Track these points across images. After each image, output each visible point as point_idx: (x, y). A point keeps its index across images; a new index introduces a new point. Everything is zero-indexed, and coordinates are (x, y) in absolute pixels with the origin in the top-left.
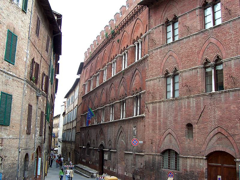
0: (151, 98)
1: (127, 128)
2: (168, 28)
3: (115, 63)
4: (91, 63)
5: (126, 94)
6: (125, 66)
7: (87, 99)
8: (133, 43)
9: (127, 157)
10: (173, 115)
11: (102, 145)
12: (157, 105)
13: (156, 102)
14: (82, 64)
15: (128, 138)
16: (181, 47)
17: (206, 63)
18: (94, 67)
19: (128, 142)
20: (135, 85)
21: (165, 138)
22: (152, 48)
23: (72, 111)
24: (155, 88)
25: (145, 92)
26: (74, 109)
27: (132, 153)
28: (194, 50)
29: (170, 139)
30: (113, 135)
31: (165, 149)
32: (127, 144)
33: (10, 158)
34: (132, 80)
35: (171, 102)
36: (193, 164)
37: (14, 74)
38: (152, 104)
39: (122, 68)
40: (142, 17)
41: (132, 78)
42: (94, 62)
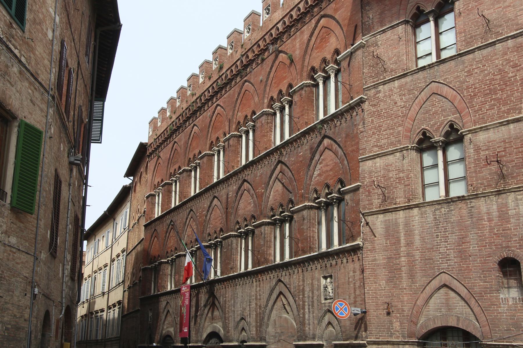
0: (380, 201)
1: (301, 283)
3: (178, 184)
4: (173, 142)
5: (291, 201)
6: (194, 190)
7: (161, 228)
8: (210, 149)
10: (453, 238)
11: (214, 335)
12: (398, 216)
15: (306, 307)
16: (469, 71)
17: (420, 142)
18: (181, 151)
19: (307, 316)
20: (319, 175)
21: (431, 297)
23: (90, 278)
24: (391, 175)
25: (357, 189)
26: (113, 261)
29: (447, 300)
30: (253, 305)
31: (432, 326)
32: (302, 323)
35: (445, 206)
39: (213, 179)
40: (336, 10)
41: (312, 159)
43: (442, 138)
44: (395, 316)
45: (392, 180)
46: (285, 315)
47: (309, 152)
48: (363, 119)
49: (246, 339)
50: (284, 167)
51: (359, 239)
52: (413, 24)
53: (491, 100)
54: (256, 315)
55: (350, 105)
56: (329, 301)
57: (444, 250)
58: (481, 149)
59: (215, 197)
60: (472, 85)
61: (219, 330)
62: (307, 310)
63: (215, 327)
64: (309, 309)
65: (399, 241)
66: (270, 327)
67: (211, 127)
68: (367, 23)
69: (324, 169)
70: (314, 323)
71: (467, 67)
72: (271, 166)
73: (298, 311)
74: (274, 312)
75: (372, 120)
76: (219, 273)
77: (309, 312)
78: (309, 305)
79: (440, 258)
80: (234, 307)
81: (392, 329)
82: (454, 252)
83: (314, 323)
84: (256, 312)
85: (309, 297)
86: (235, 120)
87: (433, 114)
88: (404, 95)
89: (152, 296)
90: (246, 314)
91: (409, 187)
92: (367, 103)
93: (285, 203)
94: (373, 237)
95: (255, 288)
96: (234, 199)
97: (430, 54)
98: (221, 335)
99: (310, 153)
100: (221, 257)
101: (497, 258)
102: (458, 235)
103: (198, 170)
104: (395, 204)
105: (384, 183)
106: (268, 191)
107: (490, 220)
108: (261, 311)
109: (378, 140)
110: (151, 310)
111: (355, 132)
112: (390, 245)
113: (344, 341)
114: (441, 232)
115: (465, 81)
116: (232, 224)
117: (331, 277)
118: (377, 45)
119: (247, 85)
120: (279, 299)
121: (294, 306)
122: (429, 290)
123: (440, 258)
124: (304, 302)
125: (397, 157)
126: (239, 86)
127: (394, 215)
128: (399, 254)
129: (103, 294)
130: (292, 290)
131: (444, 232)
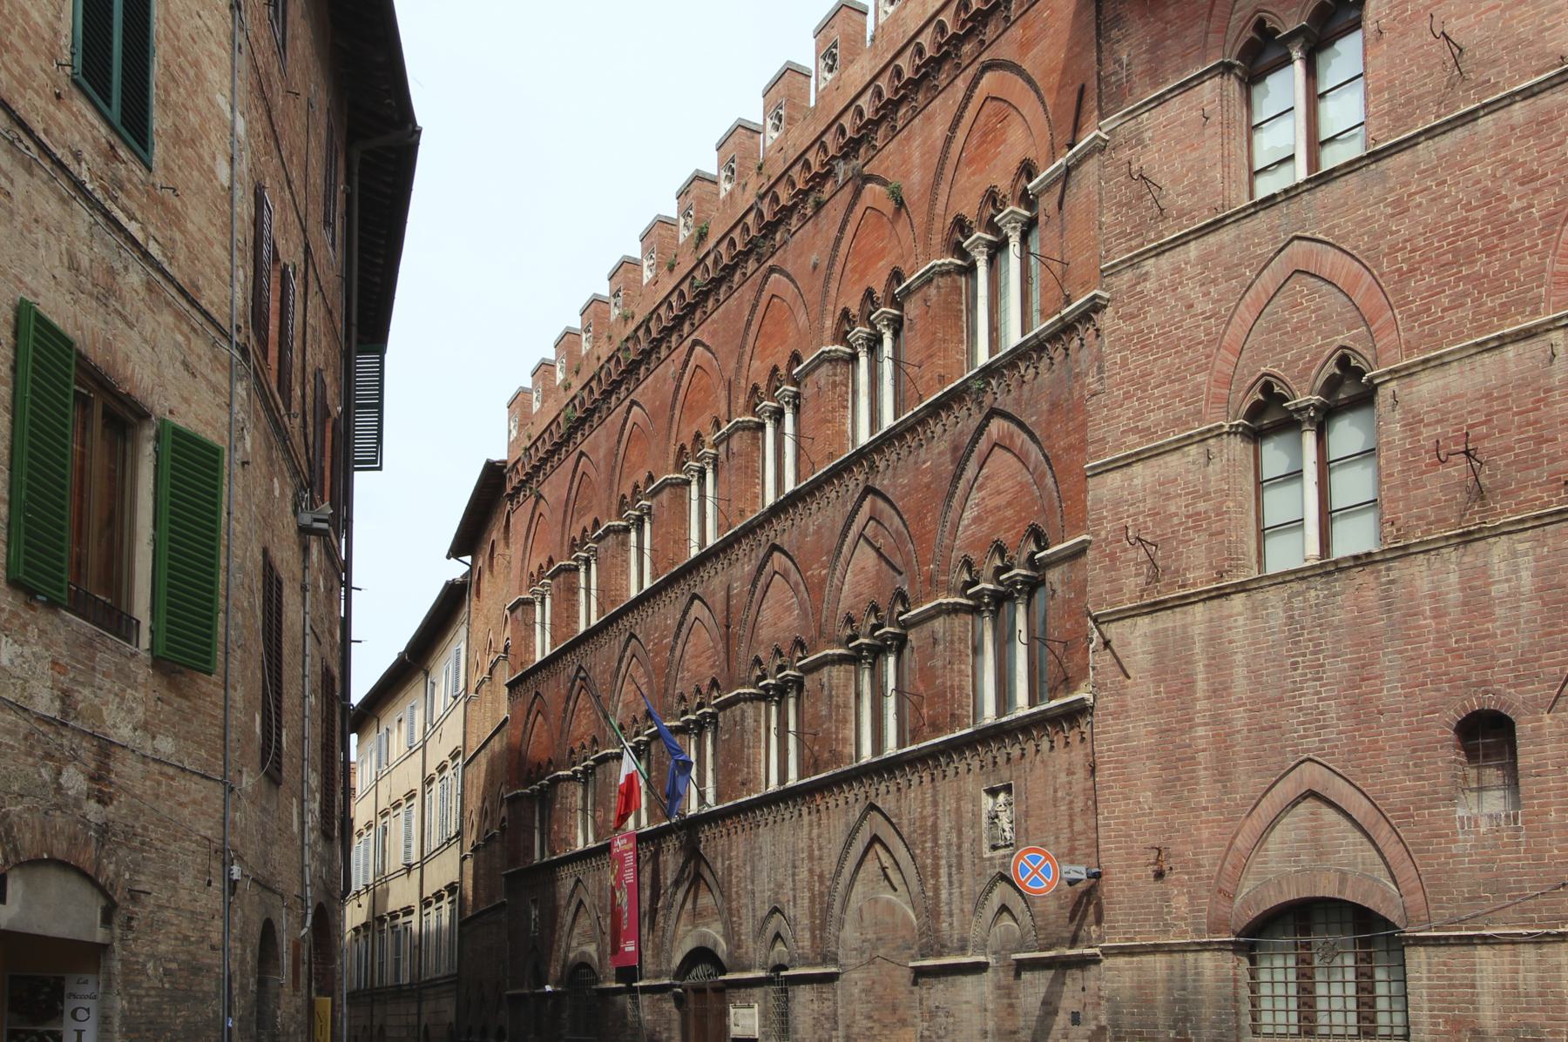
1: (929, 810)
2: (1274, 82)
4: (575, 455)
5: (901, 597)
7: (553, 689)
9: (938, 992)
10: (1337, 669)
11: (702, 955)
13: (1184, 601)
14: (493, 475)
15: (943, 871)
16: (1398, 202)
17: (1256, 411)
18: (598, 476)
19: (944, 895)
20: (977, 520)
21: (1272, 825)
22: (1133, 243)
24: (1173, 509)
25: (1079, 552)
26: (428, 781)
27: (982, 959)
28: (1516, 204)
29: (1316, 831)
30: (803, 874)
31: (1273, 900)
32: (932, 913)
33: (168, 914)
34: (951, 495)
35: (1318, 582)
36: (1529, 980)
37: (154, 249)
38: (1147, 619)
40: (1025, 46)
41: (957, 477)
42: (597, 442)
43: (1316, 398)
44: (1177, 880)
45: (1175, 520)
46: (888, 895)
47: (948, 457)
48: (1099, 358)
49: (786, 960)
50: (881, 504)
51: (1083, 685)
52: (1245, 73)
53: (1458, 280)
54: (812, 900)
55: (1062, 319)
56: (1001, 852)
57: (1312, 701)
58: (1422, 421)
59: (695, 597)
60: (1406, 241)
61: (716, 943)
62: (944, 879)
63: (705, 935)
64: (950, 875)
65: (1190, 683)
66: (847, 927)
67: (678, 406)
68: (1113, 79)
69: (991, 503)
70: (962, 910)
71: (1392, 190)
72: (844, 504)
73: (922, 882)
74: (858, 888)
75: (1124, 359)
76: (710, 798)
77: (951, 883)
78: (950, 866)
79: (1300, 724)
80: (753, 883)
81: (1169, 913)
82: (1340, 705)
83: (962, 910)
84: (811, 890)
85: (949, 845)
86: (743, 382)
87: (1294, 330)
88: (1214, 281)
89: (537, 865)
90: (783, 899)
91: (1220, 538)
92: (1109, 310)
93: (883, 602)
94: (1121, 677)
95: (806, 829)
96: (746, 599)
97: (1291, 158)
98: (719, 954)
99: (952, 462)
100: (714, 755)
101: (1453, 715)
102: (1351, 660)
103: (647, 526)
104: (1183, 586)
105: (1153, 532)
106: (838, 573)
107: (1438, 614)
108: (823, 888)
109: (1139, 414)
110: (534, 901)
111: (1076, 395)
112: (1168, 698)
113: (1041, 950)
114: (1304, 655)
115: (1386, 231)
116: (743, 667)
117: (1008, 789)
118: (1140, 142)
119: (777, 281)
120: (871, 855)
121: (911, 872)
122: (1267, 808)
123: (1300, 724)
124: (936, 858)
125: (1190, 459)
126: (754, 284)
127: (1178, 616)
128: (1190, 720)
129: (409, 868)
130: (905, 831)
131: (1313, 653)
